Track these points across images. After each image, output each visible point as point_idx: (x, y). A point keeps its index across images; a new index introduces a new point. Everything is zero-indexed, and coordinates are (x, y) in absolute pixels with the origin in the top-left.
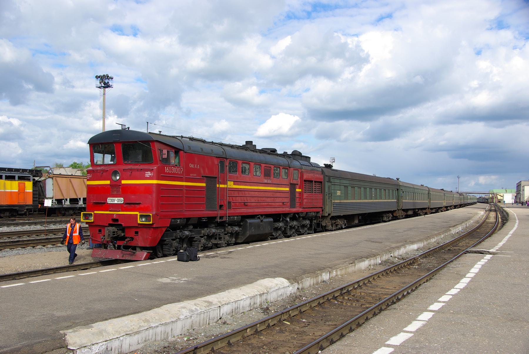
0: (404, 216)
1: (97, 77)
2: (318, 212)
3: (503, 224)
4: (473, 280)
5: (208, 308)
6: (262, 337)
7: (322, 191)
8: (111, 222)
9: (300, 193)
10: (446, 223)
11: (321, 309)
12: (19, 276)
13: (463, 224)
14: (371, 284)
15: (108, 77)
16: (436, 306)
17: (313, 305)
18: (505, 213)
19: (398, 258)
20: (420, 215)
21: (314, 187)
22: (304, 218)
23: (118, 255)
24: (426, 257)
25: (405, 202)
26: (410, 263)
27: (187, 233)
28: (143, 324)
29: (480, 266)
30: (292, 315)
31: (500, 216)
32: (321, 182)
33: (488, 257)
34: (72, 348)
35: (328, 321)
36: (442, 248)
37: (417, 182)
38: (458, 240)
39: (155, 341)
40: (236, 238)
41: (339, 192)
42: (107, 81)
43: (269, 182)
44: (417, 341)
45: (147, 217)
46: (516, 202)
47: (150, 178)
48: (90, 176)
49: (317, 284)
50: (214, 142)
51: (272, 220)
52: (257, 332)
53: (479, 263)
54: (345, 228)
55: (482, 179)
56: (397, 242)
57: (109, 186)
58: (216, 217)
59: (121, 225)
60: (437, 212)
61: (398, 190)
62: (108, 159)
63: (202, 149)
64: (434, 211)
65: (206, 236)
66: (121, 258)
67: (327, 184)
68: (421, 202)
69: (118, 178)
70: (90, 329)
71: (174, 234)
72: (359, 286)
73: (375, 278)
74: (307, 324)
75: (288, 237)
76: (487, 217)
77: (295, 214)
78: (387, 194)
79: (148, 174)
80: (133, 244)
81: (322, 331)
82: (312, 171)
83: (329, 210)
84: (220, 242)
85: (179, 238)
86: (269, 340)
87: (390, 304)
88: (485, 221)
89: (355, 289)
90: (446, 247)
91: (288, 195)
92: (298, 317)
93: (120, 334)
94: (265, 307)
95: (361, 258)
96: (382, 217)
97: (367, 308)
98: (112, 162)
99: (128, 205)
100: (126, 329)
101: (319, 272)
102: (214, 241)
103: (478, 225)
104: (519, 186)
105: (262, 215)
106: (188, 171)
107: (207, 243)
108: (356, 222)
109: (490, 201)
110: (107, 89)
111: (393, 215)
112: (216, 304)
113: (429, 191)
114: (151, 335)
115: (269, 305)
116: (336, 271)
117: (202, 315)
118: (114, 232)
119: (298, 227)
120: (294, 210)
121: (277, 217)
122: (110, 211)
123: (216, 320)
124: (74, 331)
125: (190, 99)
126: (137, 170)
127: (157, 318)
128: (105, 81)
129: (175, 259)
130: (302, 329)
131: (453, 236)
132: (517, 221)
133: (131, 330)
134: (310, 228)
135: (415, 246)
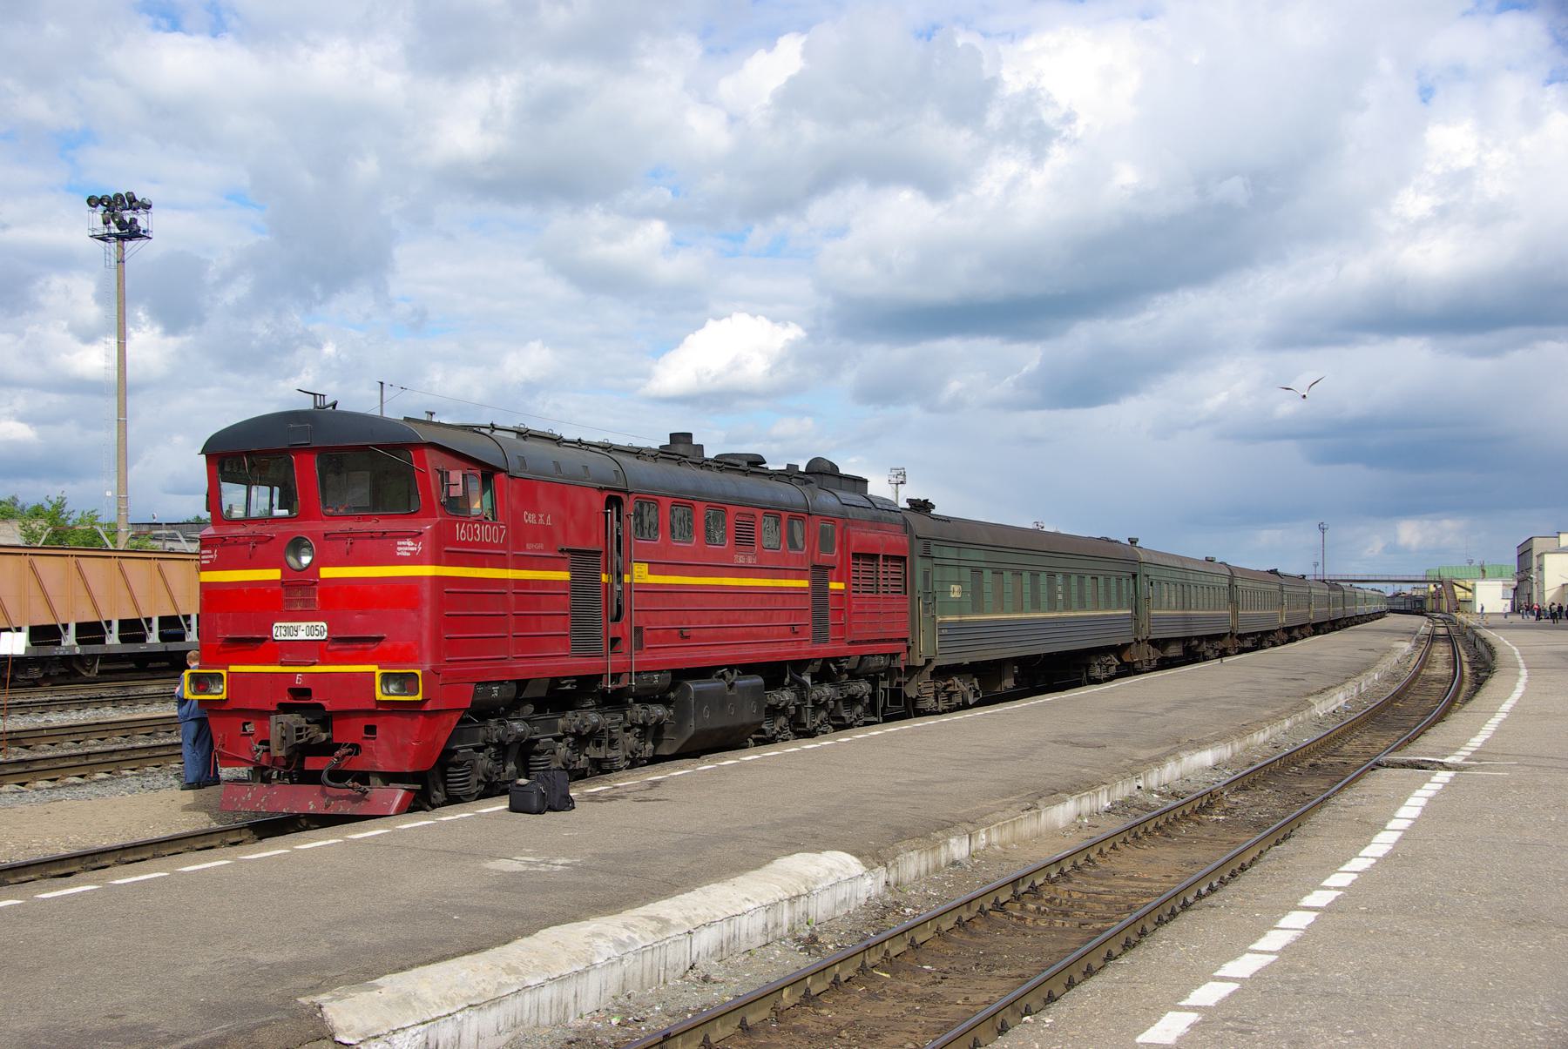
0: (1154, 663)
1: (93, 202)
2: (893, 656)
3: (1479, 684)
4: (1407, 835)
5: (660, 937)
6: (825, 1011)
7: (905, 586)
8: (287, 699)
9: (839, 594)
10: (1295, 684)
11: (966, 938)
12: (15, 876)
13: (1350, 685)
14: (1096, 867)
15: (132, 203)
16: (1319, 898)
17: (945, 927)
18: (1482, 648)
19: (1160, 793)
20: (1206, 659)
21: (881, 576)
22: (854, 675)
23: (310, 800)
24: (1244, 789)
25: (1158, 617)
26: (1191, 810)
27: (518, 727)
28: (504, 979)
29: (1423, 802)
30: (893, 953)
31: (1465, 658)
32: (903, 559)
33: (1443, 776)
34: (346, 1041)
35: (998, 968)
36: (1290, 760)
37: (1193, 546)
38: (1338, 737)
39: (537, 1026)
40: (657, 742)
41: (956, 588)
42: (128, 216)
43: (751, 561)
44: (1290, 969)
45: (407, 681)
46: (1515, 609)
47: (413, 560)
48: (210, 555)
49: (937, 869)
50: (585, 439)
51: (759, 680)
52: (808, 999)
53: (1418, 792)
54: (977, 705)
55: (1410, 533)
56: (1153, 744)
57: (278, 587)
58: (599, 678)
59: (320, 707)
60: (1257, 646)
61: (1134, 576)
62: (262, 499)
63: (557, 465)
64: (1248, 644)
65: (573, 735)
66: (322, 811)
67: (920, 565)
68: (1209, 614)
69: (306, 560)
70: (376, 993)
71: (482, 732)
72: (1061, 873)
73: (1105, 850)
74: (939, 976)
75: (811, 734)
76: (1425, 661)
77: (826, 661)
78: (1101, 590)
79: (406, 547)
80: (359, 764)
81: (990, 992)
82: (876, 522)
83: (927, 647)
84: (613, 754)
85: (494, 745)
86: (849, 1018)
87: (1178, 909)
88: (1417, 674)
89: (1053, 882)
90: (1304, 758)
91: (807, 604)
92: (908, 959)
93: (454, 1004)
94: (806, 935)
95: (1055, 793)
96: (1088, 666)
97: (1100, 931)
98: (285, 512)
99: (341, 646)
100: (465, 992)
101: (939, 834)
102: (593, 752)
103: (1395, 687)
104: (1525, 553)
105: (731, 668)
106: (518, 533)
107: (575, 757)
108: (1009, 683)
109: (1429, 605)
110: (129, 244)
111: (1120, 659)
112: (679, 926)
113: (1232, 577)
114: (527, 1008)
115: (813, 929)
116: (988, 832)
117: (648, 955)
118: (299, 730)
119: (836, 702)
120: (827, 649)
121: (774, 673)
122: (282, 664)
123: (681, 971)
124: (340, 998)
125: (424, 269)
126: (372, 536)
127: (536, 962)
128: (121, 217)
129: (500, 805)
130: (929, 990)
131: (1320, 723)
132: (1524, 672)
133: (480, 995)
134: (872, 709)
135: (1207, 757)
